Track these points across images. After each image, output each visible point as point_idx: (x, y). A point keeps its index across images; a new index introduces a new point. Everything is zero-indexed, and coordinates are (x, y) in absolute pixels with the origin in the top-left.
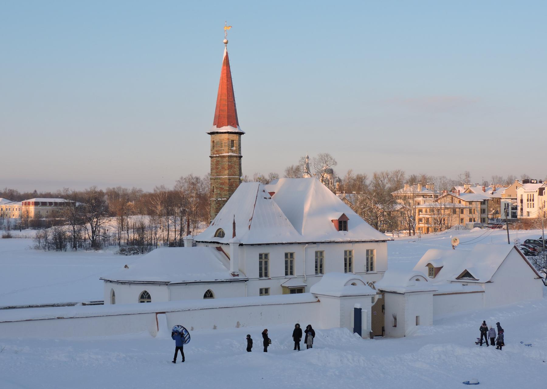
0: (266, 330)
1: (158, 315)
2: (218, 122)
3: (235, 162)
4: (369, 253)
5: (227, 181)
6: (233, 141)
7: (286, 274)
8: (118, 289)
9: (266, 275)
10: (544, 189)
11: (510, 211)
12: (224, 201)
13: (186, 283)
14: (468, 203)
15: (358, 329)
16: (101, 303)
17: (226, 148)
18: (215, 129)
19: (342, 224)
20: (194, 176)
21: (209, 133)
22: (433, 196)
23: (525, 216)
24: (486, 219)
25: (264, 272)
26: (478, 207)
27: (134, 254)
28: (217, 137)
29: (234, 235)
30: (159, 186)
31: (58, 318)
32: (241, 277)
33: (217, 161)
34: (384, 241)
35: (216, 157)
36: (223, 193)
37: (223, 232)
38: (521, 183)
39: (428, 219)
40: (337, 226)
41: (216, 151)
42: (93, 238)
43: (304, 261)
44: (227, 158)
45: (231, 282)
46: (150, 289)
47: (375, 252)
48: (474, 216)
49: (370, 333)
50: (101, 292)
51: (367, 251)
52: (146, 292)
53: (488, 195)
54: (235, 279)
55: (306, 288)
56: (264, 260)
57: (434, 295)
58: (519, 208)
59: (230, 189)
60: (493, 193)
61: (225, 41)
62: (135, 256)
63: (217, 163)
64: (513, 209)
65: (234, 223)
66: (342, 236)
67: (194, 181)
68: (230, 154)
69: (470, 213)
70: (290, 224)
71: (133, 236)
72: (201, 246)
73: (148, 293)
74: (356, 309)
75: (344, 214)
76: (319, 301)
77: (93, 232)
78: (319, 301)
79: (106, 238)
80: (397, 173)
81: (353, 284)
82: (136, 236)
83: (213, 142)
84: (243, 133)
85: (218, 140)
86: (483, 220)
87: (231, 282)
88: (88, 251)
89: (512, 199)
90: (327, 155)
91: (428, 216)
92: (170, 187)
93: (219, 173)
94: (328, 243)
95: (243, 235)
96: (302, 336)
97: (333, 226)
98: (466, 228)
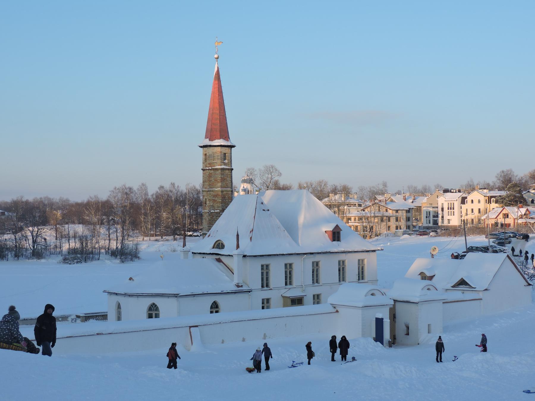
0: (310, 343)
1: (192, 329)
2: (210, 135)
3: (227, 175)
4: (361, 262)
5: (220, 193)
6: (225, 154)
7: (286, 284)
8: (123, 300)
9: (267, 286)
10: (466, 198)
11: (431, 219)
12: (216, 213)
13: (194, 295)
14: (394, 212)
15: (379, 338)
16: (103, 317)
17: (219, 161)
18: (207, 142)
19: (336, 235)
20: (127, 186)
21: (201, 147)
22: (357, 205)
23: (446, 223)
24: (411, 227)
25: (265, 283)
26: (403, 215)
27: (77, 262)
28: (210, 150)
29: (238, 247)
30: (93, 196)
31: (97, 334)
32: (245, 288)
33: (209, 172)
34: (374, 251)
35: (209, 169)
36: (216, 205)
37: (222, 244)
38: (442, 192)
39: (357, 226)
40: (331, 237)
41: (209, 164)
42: (34, 247)
43: (302, 271)
44: (220, 171)
45: (235, 293)
46: (158, 301)
47: (366, 262)
48: (400, 224)
49: (389, 342)
50: (105, 305)
51: (359, 260)
52: (154, 304)
53: (409, 204)
54: (240, 290)
55: (305, 297)
56: (265, 269)
57: (443, 303)
58: (440, 216)
59: (222, 201)
60: (412, 202)
61: (216, 56)
62: (79, 265)
63: (210, 176)
64: (434, 217)
65: (238, 235)
66: (335, 247)
67: (128, 191)
68: (223, 167)
69: (397, 220)
70: (288, 235)
71: (74, 244)
72: (248, 259)
73: (156, 305)
74: (377, 319)
75: (337, 226)
76: (337, 311)
77: (34, 242)
78: (337, 311)
79: (46, 247)
80: (320, 183)
81: (372, 295)
82: (78, 245)
83: (206, 154)
84: (234, 146)
85: (210, 153)
86: (408, 227)
87: (235, 293)
88: (30, 261)
89: (433, 207)
90: (272, 167)
91: (358, 224)
92: (103, 197)
93: (211, 185)
94: (324, 253)
95: (246, 247)
96: (340, 347)
97: (327, 239)
98: (395, 235)
